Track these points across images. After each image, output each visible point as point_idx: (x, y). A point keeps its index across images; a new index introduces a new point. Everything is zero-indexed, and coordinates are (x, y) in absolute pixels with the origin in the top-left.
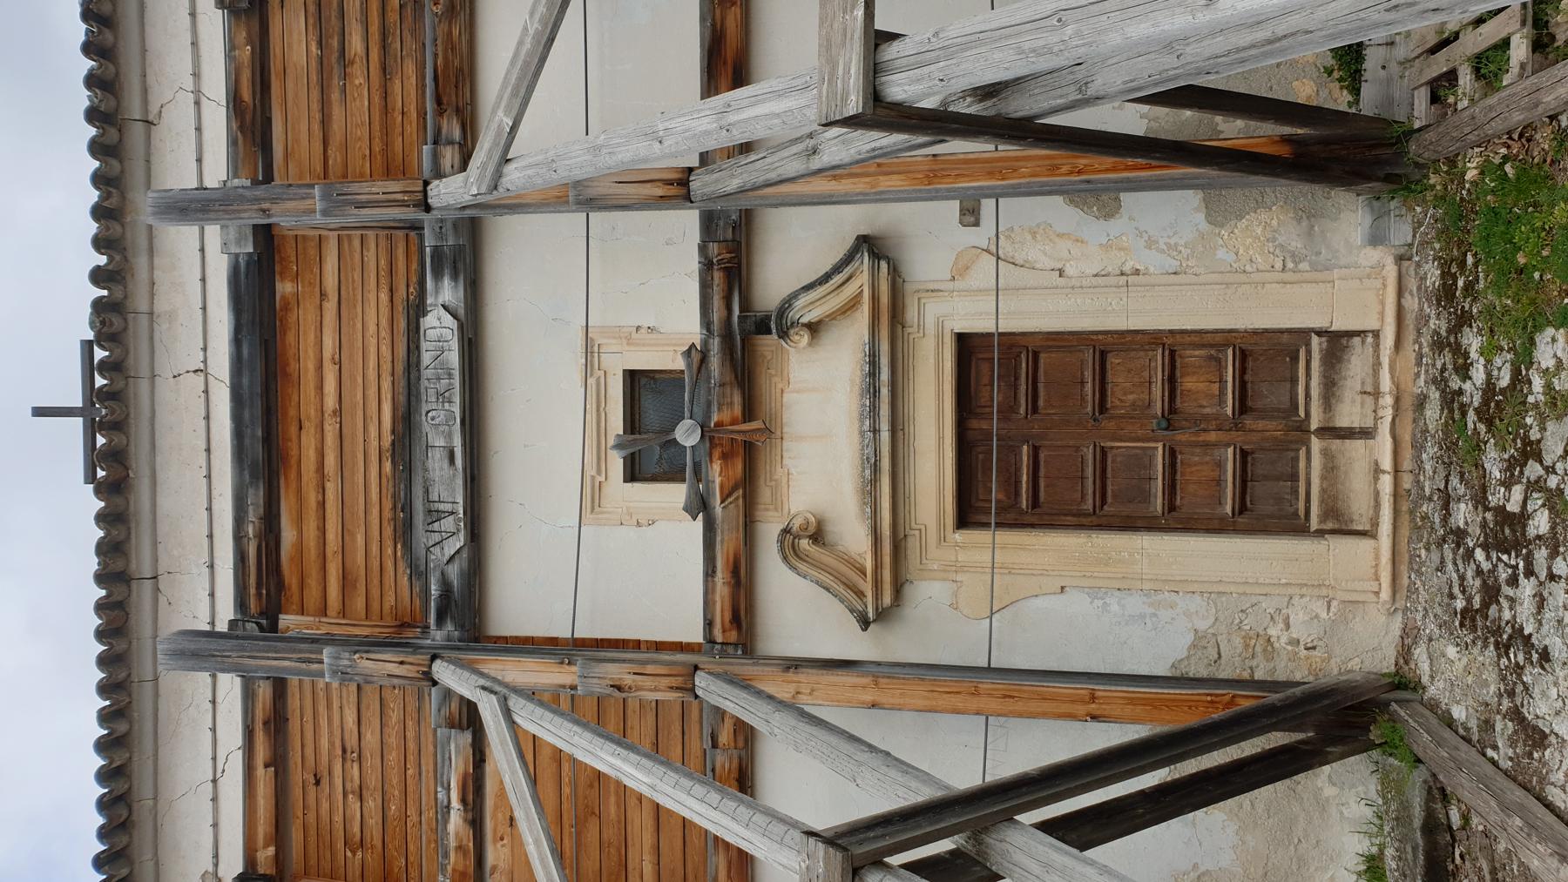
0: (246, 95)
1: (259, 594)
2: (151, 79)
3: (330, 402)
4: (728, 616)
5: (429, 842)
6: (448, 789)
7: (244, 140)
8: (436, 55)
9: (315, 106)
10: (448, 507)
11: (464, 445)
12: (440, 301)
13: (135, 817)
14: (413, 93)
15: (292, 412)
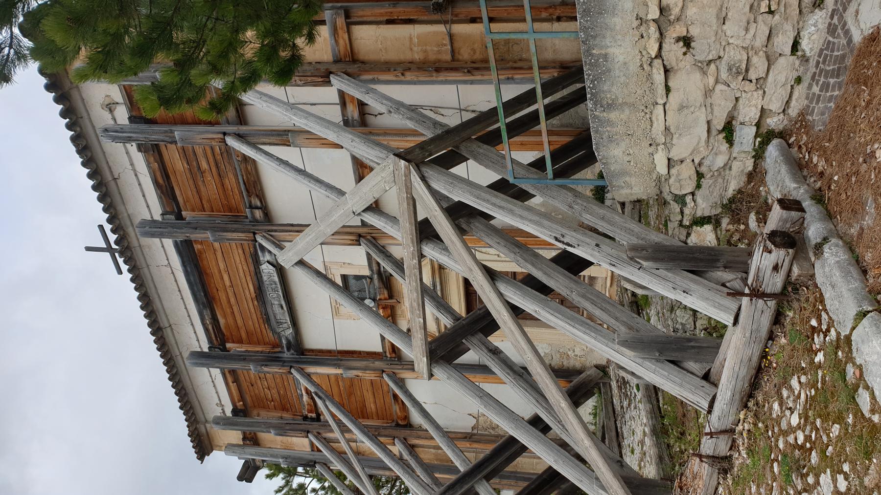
0: (161, 181)
1: (217, 340)
2: (111, 164)
3: (228, 283)
4: (391, 350)
5: (297, 401)
6: (301, 390)
7: (165, 197)
8: (242, 176)
9: (193, 187)
10: (285, 321)
11: (286, 303)
12: (266, 260)
13: (187, 391)
14: (235, 185)
15: (212, 285)
